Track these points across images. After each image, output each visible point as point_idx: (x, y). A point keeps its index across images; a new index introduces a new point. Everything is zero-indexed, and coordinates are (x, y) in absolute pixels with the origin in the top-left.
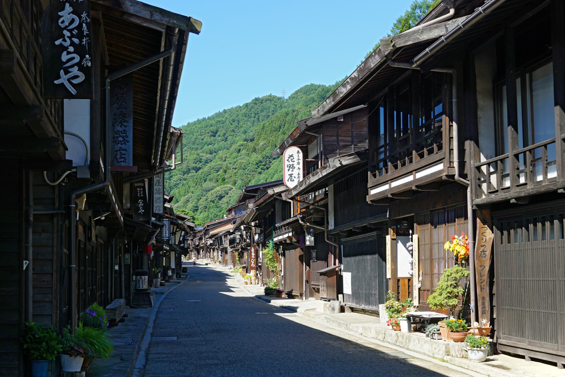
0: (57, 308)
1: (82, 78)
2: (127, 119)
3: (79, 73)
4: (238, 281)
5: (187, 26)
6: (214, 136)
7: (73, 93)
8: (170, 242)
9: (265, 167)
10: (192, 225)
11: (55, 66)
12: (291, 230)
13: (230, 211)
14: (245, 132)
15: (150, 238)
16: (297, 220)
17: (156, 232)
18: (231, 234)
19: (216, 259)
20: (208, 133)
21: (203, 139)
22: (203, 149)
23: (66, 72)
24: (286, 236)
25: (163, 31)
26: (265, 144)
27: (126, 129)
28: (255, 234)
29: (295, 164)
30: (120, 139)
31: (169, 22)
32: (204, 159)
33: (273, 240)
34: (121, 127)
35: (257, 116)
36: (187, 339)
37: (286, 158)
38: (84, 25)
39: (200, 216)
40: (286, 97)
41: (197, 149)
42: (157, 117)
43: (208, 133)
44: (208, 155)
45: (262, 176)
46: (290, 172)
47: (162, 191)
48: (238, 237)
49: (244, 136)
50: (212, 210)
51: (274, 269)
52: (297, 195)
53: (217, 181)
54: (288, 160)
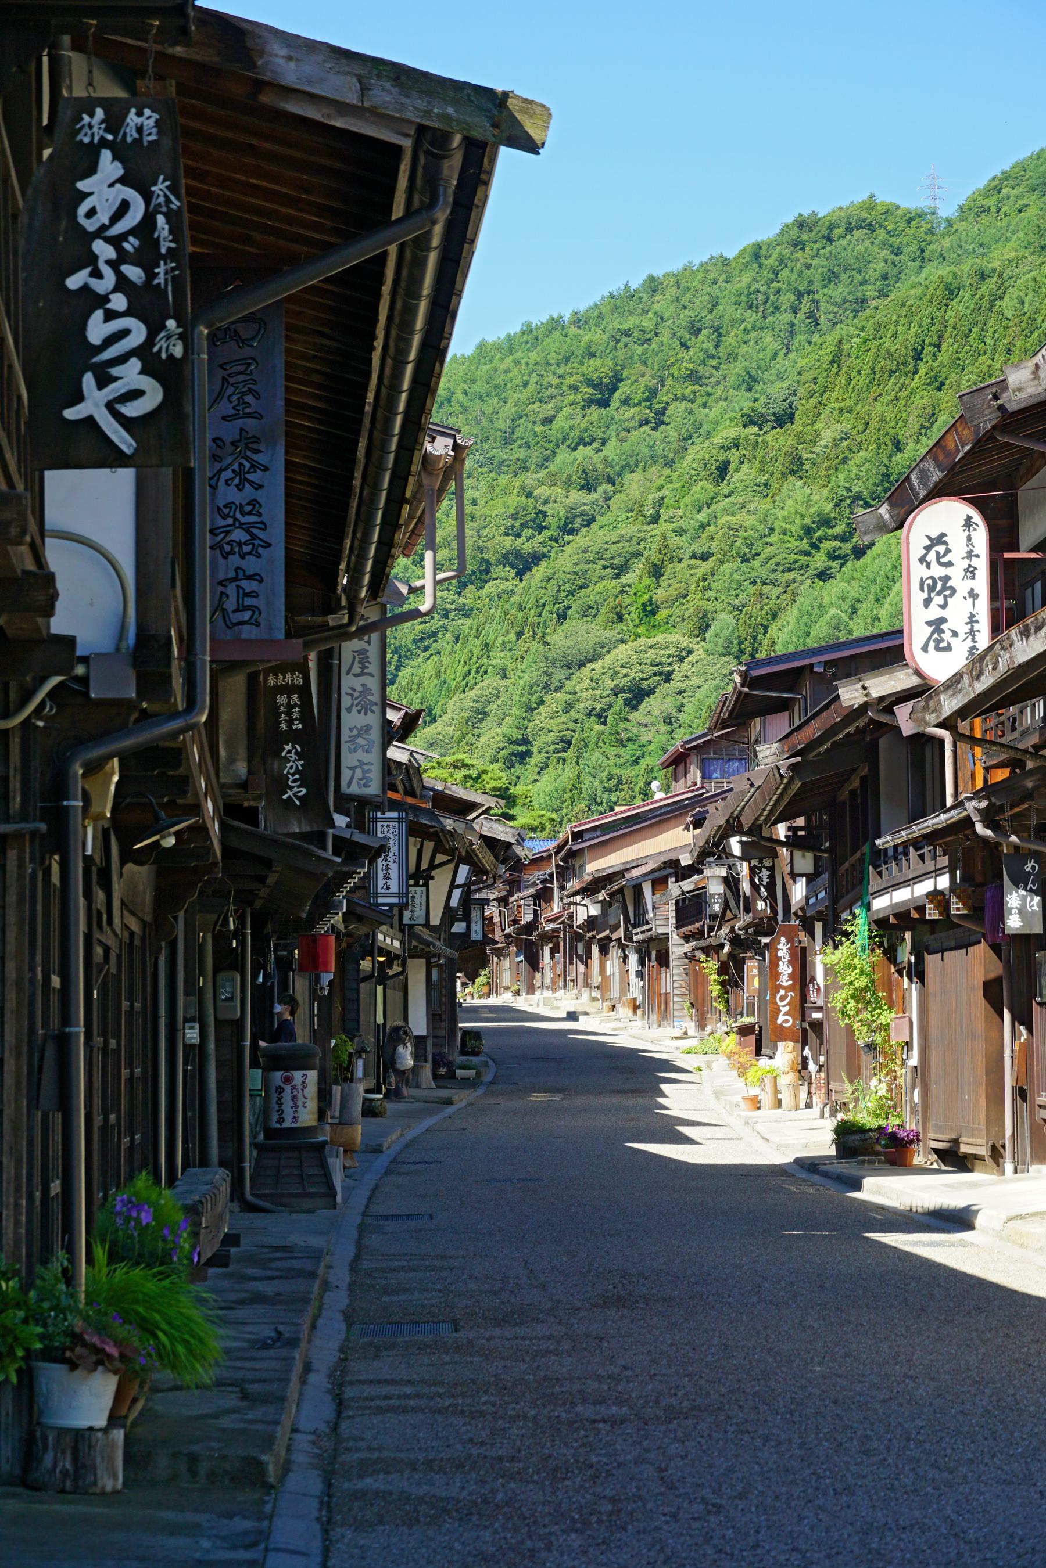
0: (18, 1189)
1: (153, 396)
2: (259, 458)
3: (147, 383)
4: (717, 1094)
5: (495, 125)
6: (604, 403)
7: (124, 448)
8: (407, 914)
9: (847, 548)
10: (501, 832)
11: (67, 360)
12: (944, 861)
13: (678, 762)
14: (750, 382)
15: (324, 906)
16: (967, 823)
17: (350, 875)
18: (682, 873)
19: (615, 991)
20: (575, 388)
21: (549, 420)
22: (552, 467)
23: (103, 381)
24: (924, 887)
25: (407, 143)
26: (846, 436)
27: (260, 495)
28: (794, 876)
29: (956, 574)
30: (239, 535)
31: (428, 113)
32: (556, 511)
33: (868, 907)
34: (240, 488)
35: (806, 305)
36: (497, 1332)
37: (917, 550)
38: (161, 220)
39: (539, 787)
40: (947, 210)
41: (523, 467)
42: (367, 422)
43: (575, 388)
44: (577, 497)
45: (834, 588)
46: (934, 612)
47: (376, 698)
48: (716, 888)
49: (744, 402)
50: (593, 757)
51: (879, 1040)
52: (963, 713)
53: (620, 617)
54: (922, 560)
